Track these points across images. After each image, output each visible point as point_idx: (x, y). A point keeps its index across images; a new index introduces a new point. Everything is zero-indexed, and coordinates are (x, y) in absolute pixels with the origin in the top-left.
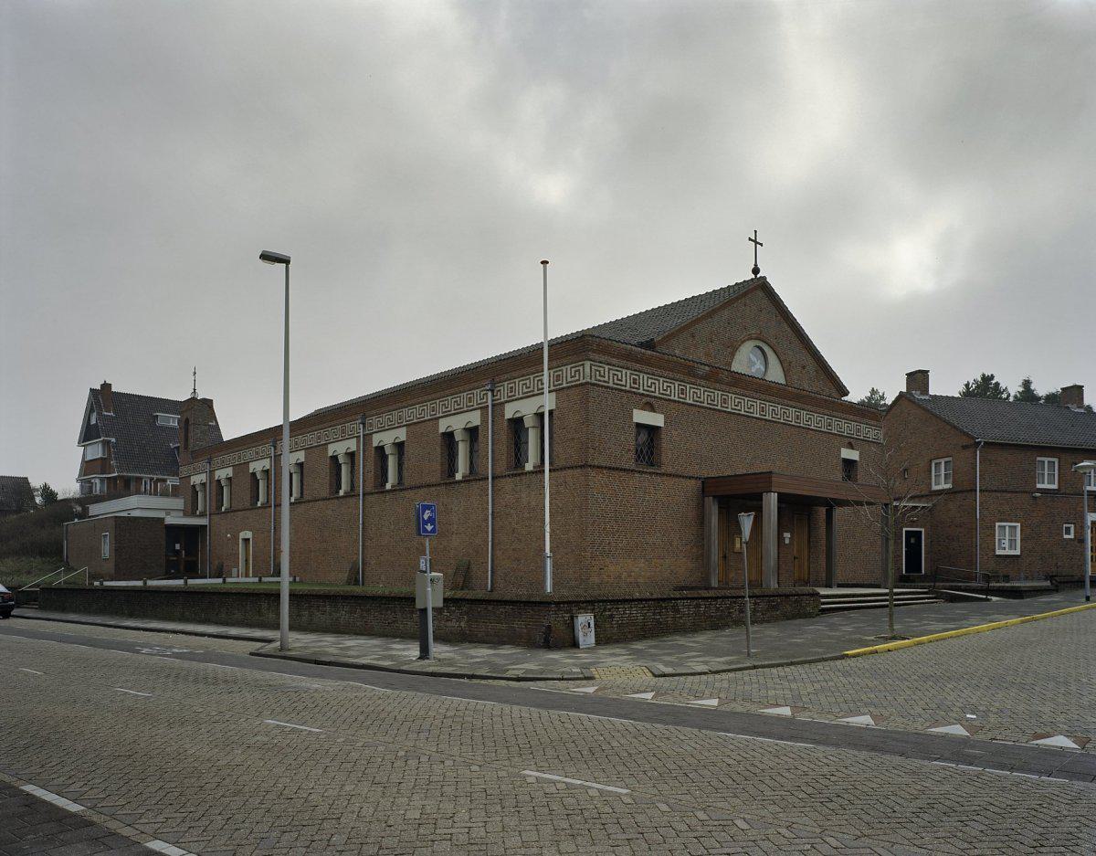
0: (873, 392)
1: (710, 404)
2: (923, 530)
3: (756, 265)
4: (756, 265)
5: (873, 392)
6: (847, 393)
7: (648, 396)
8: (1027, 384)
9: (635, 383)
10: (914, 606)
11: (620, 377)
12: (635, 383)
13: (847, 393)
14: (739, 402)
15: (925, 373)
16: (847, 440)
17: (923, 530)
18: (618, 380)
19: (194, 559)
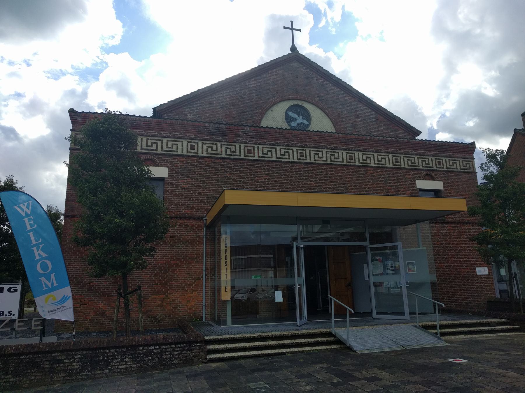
0: (15, 91)
1: (438, 168)
2: (407, 262)
3: (293, 45)
4: (293, 45)
5: (15, 91)
6: (419, 133)
7: (426, 170)
8: (314, 2)
9: (439, 164)
10: (243, 362)
11: (427, 162)
12: (397, 162)
13: (419, 133)
14: (466, 164)
15: (487, 89)
16: (423, 174)
17: (414, 261)
18: (425, 161)
19: (233, 258)
